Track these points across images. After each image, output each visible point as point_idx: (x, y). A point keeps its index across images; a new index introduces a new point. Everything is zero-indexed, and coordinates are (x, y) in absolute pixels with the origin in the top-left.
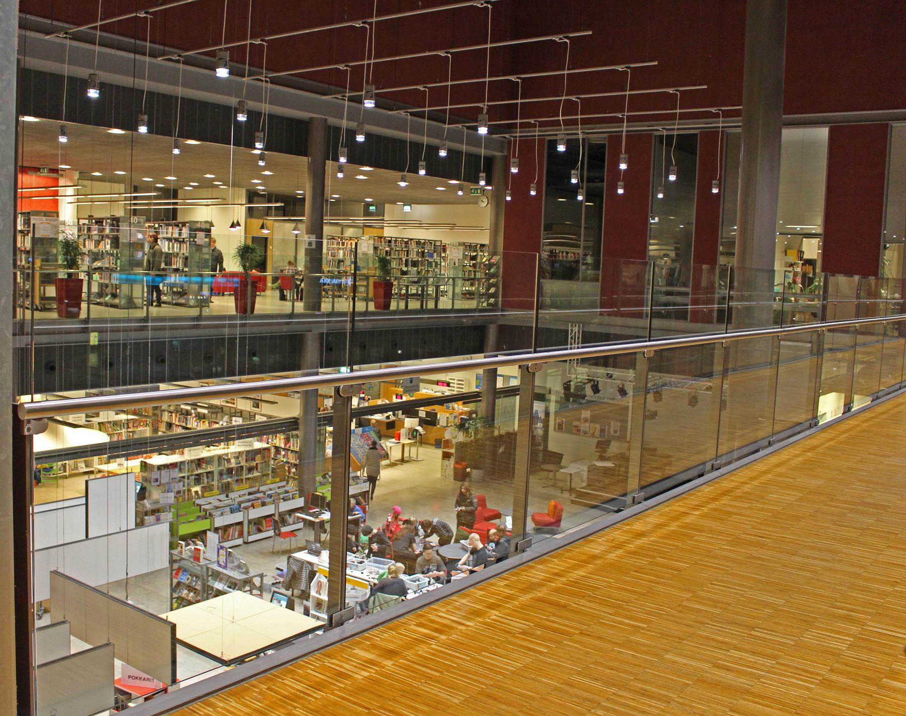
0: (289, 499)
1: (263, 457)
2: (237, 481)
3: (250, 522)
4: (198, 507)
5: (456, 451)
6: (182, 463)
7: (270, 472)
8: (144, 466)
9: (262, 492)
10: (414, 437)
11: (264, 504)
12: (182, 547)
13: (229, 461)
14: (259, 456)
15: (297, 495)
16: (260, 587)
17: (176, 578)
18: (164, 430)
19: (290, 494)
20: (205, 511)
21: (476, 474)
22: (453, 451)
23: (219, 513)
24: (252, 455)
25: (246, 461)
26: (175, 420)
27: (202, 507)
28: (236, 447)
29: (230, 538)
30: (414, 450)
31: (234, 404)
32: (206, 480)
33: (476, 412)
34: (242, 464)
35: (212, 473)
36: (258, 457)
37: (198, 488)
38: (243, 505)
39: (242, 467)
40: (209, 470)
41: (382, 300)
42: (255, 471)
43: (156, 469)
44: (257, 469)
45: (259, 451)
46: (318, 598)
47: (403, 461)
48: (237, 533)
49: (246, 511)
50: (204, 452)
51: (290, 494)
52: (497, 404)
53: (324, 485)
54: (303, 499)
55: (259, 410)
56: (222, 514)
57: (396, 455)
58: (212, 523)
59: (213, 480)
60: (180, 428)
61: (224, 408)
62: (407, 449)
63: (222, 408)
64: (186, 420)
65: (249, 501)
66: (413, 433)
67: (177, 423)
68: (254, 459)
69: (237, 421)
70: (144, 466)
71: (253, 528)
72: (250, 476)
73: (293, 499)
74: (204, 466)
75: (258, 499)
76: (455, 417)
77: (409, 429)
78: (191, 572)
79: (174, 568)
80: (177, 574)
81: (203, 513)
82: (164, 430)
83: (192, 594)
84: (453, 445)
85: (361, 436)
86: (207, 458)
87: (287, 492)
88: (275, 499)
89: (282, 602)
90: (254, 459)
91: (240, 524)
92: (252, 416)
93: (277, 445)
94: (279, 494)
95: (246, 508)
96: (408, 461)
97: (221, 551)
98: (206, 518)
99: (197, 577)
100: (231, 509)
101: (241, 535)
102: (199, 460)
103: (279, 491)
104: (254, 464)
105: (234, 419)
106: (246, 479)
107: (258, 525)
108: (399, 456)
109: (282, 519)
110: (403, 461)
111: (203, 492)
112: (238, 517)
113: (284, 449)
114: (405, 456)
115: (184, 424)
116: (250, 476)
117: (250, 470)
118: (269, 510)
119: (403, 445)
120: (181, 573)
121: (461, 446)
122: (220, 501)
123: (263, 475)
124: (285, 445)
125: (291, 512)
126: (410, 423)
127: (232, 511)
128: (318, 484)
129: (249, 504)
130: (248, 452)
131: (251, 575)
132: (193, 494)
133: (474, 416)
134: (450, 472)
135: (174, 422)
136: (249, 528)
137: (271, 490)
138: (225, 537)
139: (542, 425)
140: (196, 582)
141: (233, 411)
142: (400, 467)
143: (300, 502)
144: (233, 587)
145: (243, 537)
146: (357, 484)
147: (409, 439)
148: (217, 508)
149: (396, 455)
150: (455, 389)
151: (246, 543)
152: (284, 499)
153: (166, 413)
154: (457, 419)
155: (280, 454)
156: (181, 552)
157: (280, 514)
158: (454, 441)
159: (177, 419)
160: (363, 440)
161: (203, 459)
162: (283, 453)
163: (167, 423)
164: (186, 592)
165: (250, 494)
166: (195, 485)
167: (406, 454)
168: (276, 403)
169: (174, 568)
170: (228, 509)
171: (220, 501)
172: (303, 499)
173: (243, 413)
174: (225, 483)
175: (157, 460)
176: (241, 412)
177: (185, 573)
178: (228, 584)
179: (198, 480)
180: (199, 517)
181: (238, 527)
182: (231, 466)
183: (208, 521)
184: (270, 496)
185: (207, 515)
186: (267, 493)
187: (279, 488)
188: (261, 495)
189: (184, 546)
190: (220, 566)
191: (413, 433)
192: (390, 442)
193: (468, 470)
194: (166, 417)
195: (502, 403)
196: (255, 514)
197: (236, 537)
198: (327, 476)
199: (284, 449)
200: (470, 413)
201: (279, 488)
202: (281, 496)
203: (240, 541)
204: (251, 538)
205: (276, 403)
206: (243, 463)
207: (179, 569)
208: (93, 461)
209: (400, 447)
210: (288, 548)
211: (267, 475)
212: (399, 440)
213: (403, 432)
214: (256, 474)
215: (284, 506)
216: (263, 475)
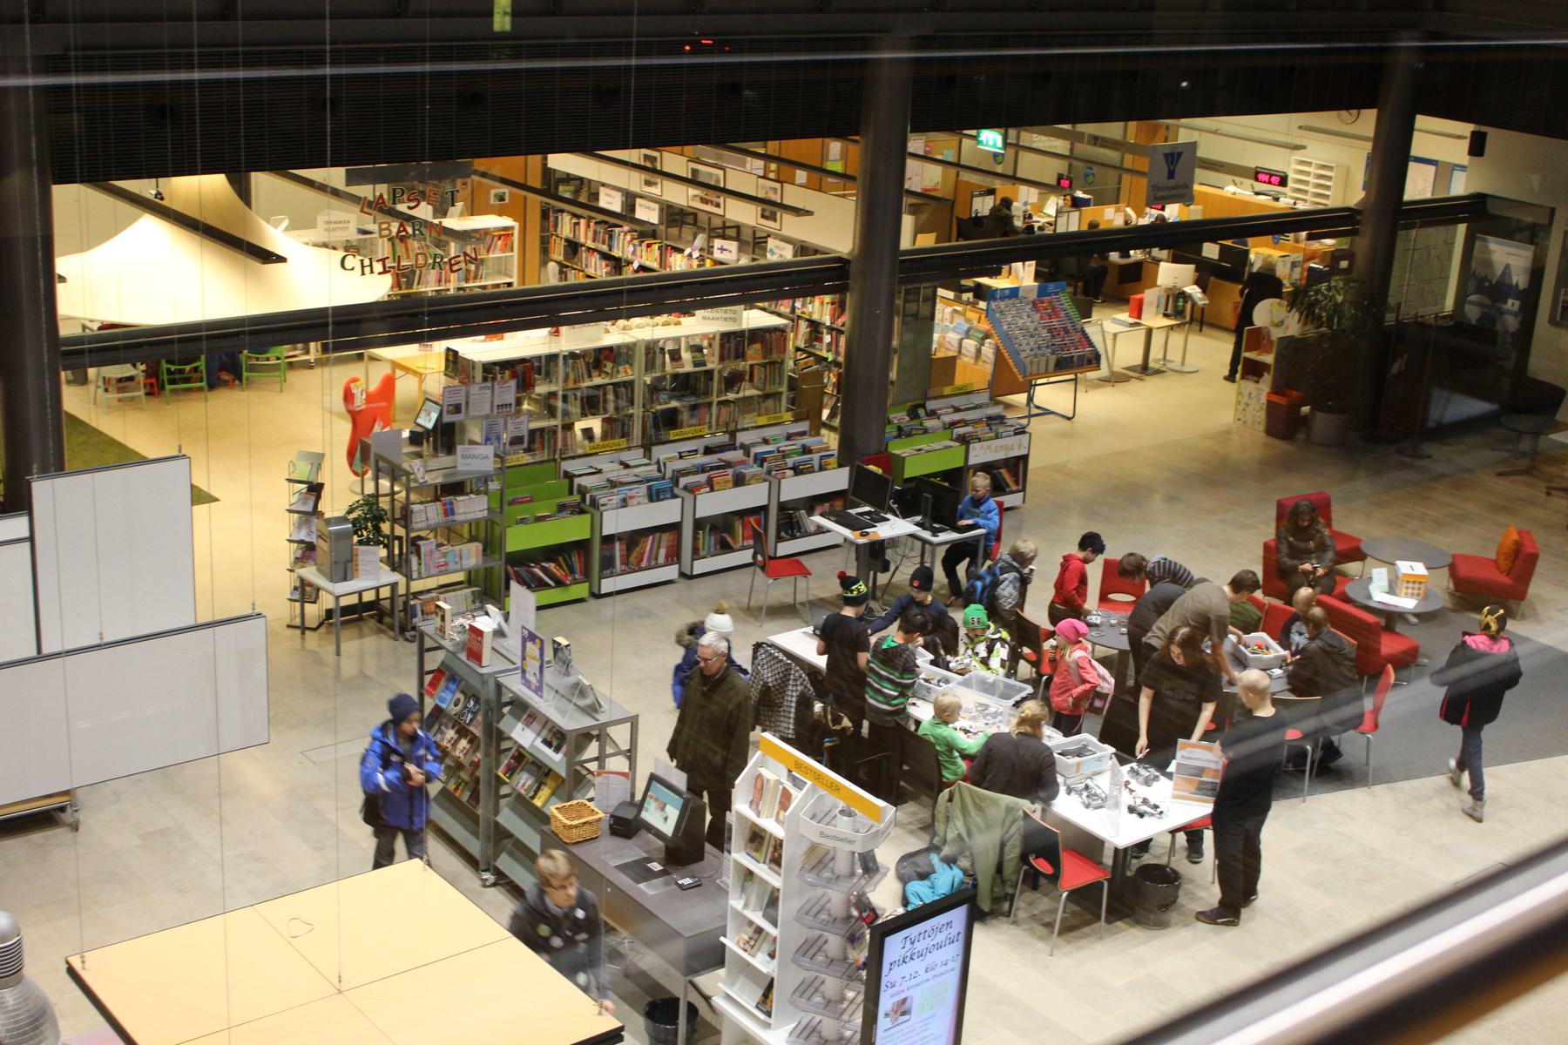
0: (811, 470)
1: (767, 350)
2: (694, 408)
3: (699, 524)
4: (567, 481)
5: (1277, 360)
6: (552, 358)
7: (784, 389)
8: (453, 358)
9: (743, 446)
10: (1179, 313)
11: (739, 481)
12: (443, 618)
13: (676, 356)
14: (757, 346)
15: (833, 461)
16: (629, 751)
17: (431, 695)
18: (561, 258)
19: (816, 457)
20: (583, 491)
21: (1323, 423)
22: (1269, 359)
23: (616, 499)
24: (734, 343)
25: (722, 359)
26: (585, 236)
27: (577, 481)
28: (702, 325)
29: (644, 564)
30: (1177, 339)
31: (718, 205)
32: (611, 406)
33: (1348, 255)
34: (710, 366)
35: (629, 385)
36: (754, 353)
37: (596, 424)
38: (683, 481)
39: (709, 374)
40: (621, 378)
41: (240, 22)
42: (745, 384)
43: (479, 375)
44: (751, 379)
45: (757, 335)
46: (754, 824)
47: (1144, 369)
48: (663, 552)
49: (688, 497)
50: (611, 334)
51: (816, 457)
52: (1399, 245)
53: (909, 435)
54: (846, 471)
55: (776, 225)
56: (624, 503)
57: (1127, 352)
58: (596, 525)
59: (632, 403)
60: (597, 256)
61: (700, 215)
62: (1158, 339)
63: (695, 215)
64: (611, 237)
65: (702, 469)
66: (1176, 303)
67: (590, 244)
68: (741, 355)
69: (728, 253)
70: (453, 358)
71: (707, 539)
72: (731, 396)
73: (821, 469)
74: (609, 367)
75: (728, 465)
76: (1294, 265)
77: (1168, 290)
78: (468, 685)
79: (428, 667)
80: (434, 684)
81: (576, 498)
82: (561, 258)
83: (463, 743)
84: (1271, 343)
85: (1034, 303)
86: (619, 347)
87: (806, 450)
88: (772, 467)
89: (669, 808)
90: (741, 355)
91: (675, 528)
92: (757, 243)
93: (816, 317)
94: (784, 456)
95: (692, 490)
96: (1158, 372)
97: (529, 645)
98: (582, 512)
99: (477, 701)
100: (649, 488)
101: (674, 556)
102: (600, 351)
103: (785, 446)
104: (742, 366)
105: (718, 243)
106: (720, 403)
107: (720, 531)
108: (1138, 359)
109: (790, 519)
110: (1144, 369)
111: (605, 436)
112: (667, 512)
113: (831, 329)
114: (1152, 355)
115: (605, 248)
116: (731, 396)
117: (733, 381)
118: (753, 495)
119: (1149, 332)
120: (443, 683)
121: (1290, 347)
122: (626, 466)
123: (766, 397)
124: (834, 318)
125: (812, 503)
126: (1172, 274)
127: (654, 496)
128: (890, 431)
129: (702, 478)
130: (726, 337)
131: (603, 718)
132: (578, 433)
133: (1344, 264)
134: (1257, 414)
135: (582, 240)
136: (695, 538)
137: (766, 441)
138: (632, 559)
139: (1517, 303)
140: (475, 714)
141: (717, 222)
142: (1134, 386)
143: (838, 479)
144: (555, 743)
145: (679, 562)
146: (997, 437)
147: (1166, 315)
148: (613, 484)
149: (1127, 352)
150: (1311, 189)
151: (687, 576)
152: (798, 471)
153: (567, 217)
154: (1298, 270)
155: (820, 340)
156: (442, 630)
157: (783, 507)
158: (1276, 334)
159: (590, 234)
160: (1037, 317)
161: (610, 349)
162: (827, 338)
163: (567, 240)
164: (451, 733)
165: (708, 451)
166: (584, 415)
167: (1156, 353)
168: (809, 213)
169: (428, 667)
170: (643, 489)
171: (626, 466)
172: (846, 471)
173: (744, 231)
174: (664, 412)
175: (476, 349)
176: (738, 227)
177: (453, 686)
178: (545, 732)
179: (591, 405)
180: (562, 508)
181: (666, 537)
182: (681, 370)
183: (587, 517)
184: (760, 460)
185: (585, 505)
186: (754, 450)
187: (789, 437)
188: (736, 455)
189: (448, 617)
190: (527, 683)
191: (1176, 303)
192: (1115, 321)
193: (1306, 409)
194: (565, 227)
195: (1416, 239)
196: (712, 504)
197: (661, 560)
198: (921, 412)
199: (831, 329)
200: (1335, 256)
201: (789, 437)
202: (790, 462)
203: (671, 572)
204: (700, 566)
205: (809, 213)
206: (713, 364)
207: (439, 673)
208: (519, 285)
209: (1140, 336)
210: (790, 600)
211: (776, 396)
212: (1139, 317)
213: (1150, 296)
214: (748, 391)
215: (795, 488)
216: (766, 397)
